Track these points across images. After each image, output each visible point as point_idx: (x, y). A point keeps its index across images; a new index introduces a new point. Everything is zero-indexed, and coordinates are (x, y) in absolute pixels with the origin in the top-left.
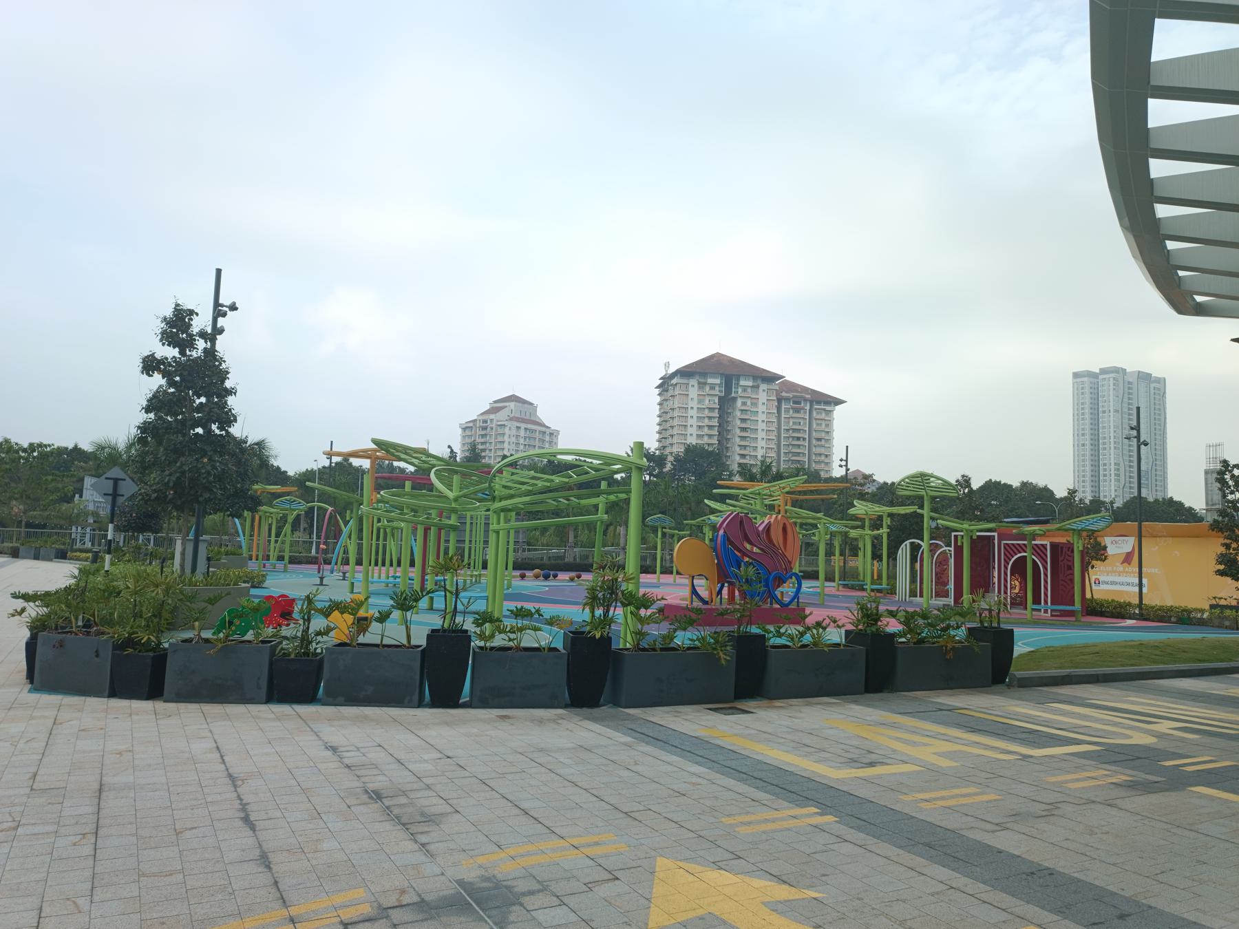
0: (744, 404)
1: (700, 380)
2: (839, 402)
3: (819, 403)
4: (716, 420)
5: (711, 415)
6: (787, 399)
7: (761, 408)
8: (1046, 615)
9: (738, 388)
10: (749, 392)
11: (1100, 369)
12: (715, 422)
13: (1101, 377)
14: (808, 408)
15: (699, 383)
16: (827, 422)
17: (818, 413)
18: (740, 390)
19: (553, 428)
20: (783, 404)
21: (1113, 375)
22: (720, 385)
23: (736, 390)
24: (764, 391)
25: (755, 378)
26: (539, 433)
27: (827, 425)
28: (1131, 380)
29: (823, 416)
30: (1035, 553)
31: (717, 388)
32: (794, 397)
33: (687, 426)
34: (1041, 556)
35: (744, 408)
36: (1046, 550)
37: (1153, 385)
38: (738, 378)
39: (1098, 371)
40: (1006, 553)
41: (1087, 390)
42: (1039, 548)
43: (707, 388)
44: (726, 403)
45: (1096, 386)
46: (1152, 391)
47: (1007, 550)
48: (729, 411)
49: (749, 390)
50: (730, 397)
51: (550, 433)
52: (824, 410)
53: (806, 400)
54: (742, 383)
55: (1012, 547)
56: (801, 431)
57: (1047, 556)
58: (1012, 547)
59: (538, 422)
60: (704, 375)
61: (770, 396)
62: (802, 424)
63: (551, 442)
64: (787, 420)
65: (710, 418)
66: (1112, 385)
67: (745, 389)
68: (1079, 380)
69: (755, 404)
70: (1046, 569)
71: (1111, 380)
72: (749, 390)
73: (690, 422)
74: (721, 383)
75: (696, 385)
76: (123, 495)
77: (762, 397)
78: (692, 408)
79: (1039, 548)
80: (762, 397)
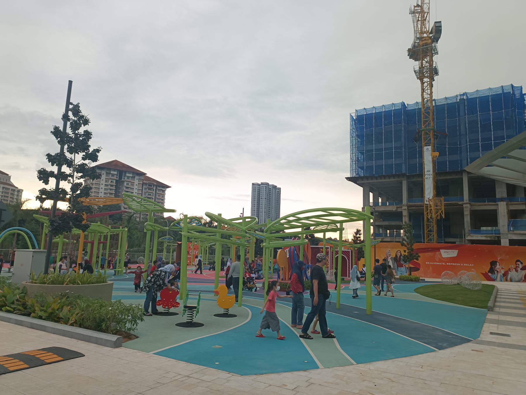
0: (128, 184)
1: (107, 172)
2: (169, 187)
3: (159, 187)
4: (114, 191)
5: (111, 188)
6: (146, 184)
7: (135, 187)
8: (349, 278)
9: (125, 177)
10: (130, 180)
11: (261, 183)
12: (113, 192)
13: (261, 186)
14: (155, 188)
15: (107, 173)
16: (163, 195)
17: (159, 191)
18: (126, 178)
19: (19, 188)
20: (144, 186)
21: (265, 185)
22: (117, 175)
23: (124, 178)
24: (137, 179)
25: (133, 173)
26: (11, 190)
27: (163, 196)
28: (270, 188)
29: (161, 192)
30: (344, 253)
31: (115, 176)
32: (149, 183)
33: (99, 192)
34: (347, 256)
35: (127, 186)
36: (349, 253)
37: (277, 190)
38: (126, 172)
39: (260, 184)
40: (348, 253)
41: (257, 190)
42: (346, 252)
43: (111, 176)
44: (119, 183)
45: (259, 189)
46: (277, 192)
47: (348, 254)
48: (120, 187)
49: (130, 178)
50: (121, 180)
51: (18, 191)
52: (162, 190)
53: (154, 185)
54: (127, 175)
55: (345, 252)
56: (151, 199)
57: (349, 255)
58: (345, 252)
59: (11, 184)
60: (110, 169)
61: (139, 182)
62: (152, 195)
63: (17, 195)
64: (145, 193)
65: (110, 189)
66: (264, 189)
67: (128, 177)
68: (254, 186)
69: (133, 185)
70: (349, 260)
71: (264, 187)
72: (130, 178)
73: (101, 190)
74: (117, 174)
75: (105, 174)
76: (4, 221)
77: (136, 182)
78: (102, 184)
79: (346, 252)
80: (136, 182)
